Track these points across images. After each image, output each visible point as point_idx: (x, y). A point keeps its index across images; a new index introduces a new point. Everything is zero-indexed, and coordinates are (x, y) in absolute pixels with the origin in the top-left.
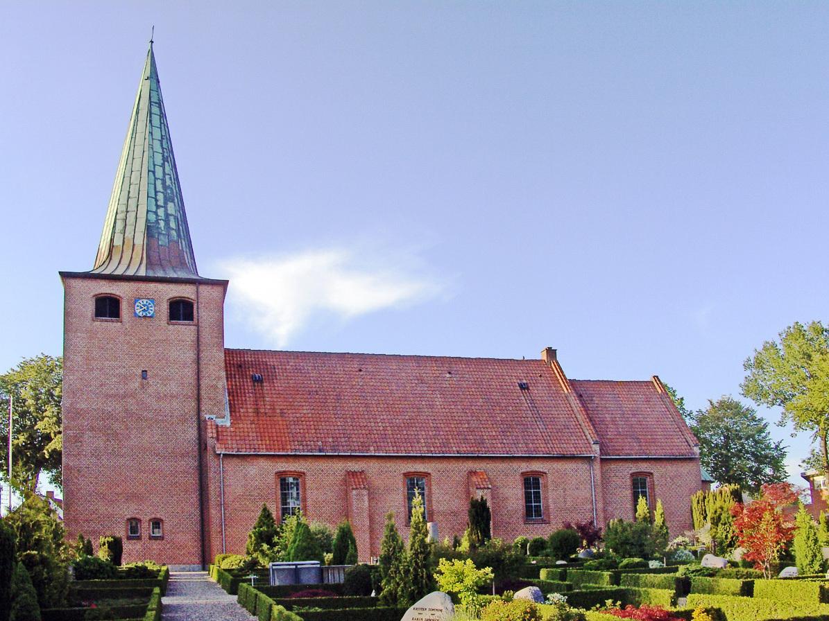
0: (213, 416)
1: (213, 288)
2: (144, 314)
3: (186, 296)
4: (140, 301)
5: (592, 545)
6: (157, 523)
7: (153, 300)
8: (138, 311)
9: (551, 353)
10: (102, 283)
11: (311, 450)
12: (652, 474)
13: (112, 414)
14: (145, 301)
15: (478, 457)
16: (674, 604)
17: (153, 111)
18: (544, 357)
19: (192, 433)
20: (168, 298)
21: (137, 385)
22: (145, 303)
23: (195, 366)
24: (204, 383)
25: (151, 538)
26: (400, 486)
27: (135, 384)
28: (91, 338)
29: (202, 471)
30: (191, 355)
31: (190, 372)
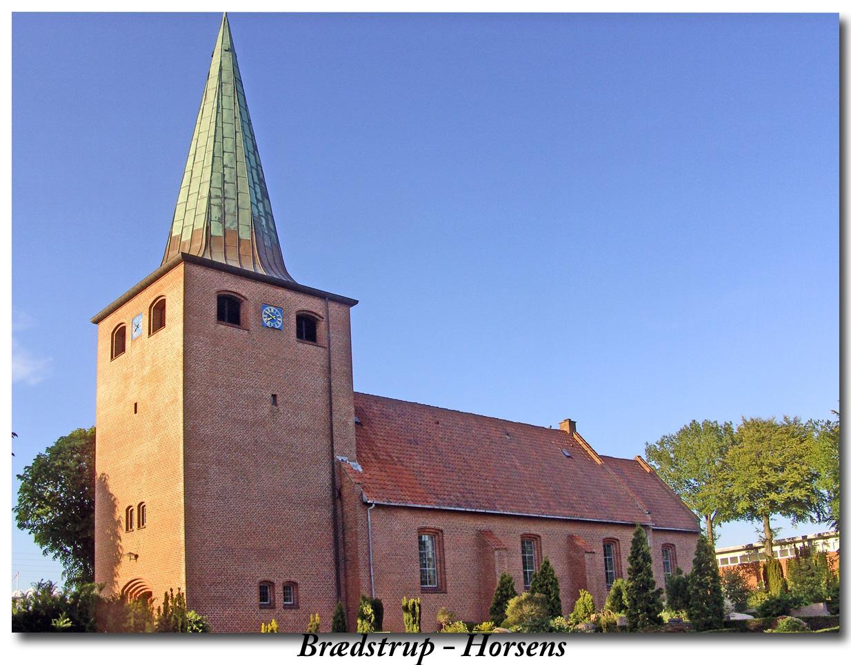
0: (345, 459)
1: (339, 307)
2: (272, 325)
3: (314, 311)
4: (268, 308)
5: (54, 540)
6: (290, 587)
7: (281, 309)
8: (265, 320)
9: (572, 424)
10: (227, 277)
11: (449, 505)
12: (673, 545)
13: (241, 446)
14: (273, 308)
15: (607, 523)
16: (491, 629)
17: (212, 203)
18: (567, 428)
19: (325, 477)
20: (297, 309)
21: (266, 411)
22: (272, 311)
23: (326, 396)
24: (336, 416)
25: (285, 607)
26: (599, 549)
27: (266, 408)
28: (215, 345)
29: (339, 527)
30: (321, 382)
31: (320, 402)
